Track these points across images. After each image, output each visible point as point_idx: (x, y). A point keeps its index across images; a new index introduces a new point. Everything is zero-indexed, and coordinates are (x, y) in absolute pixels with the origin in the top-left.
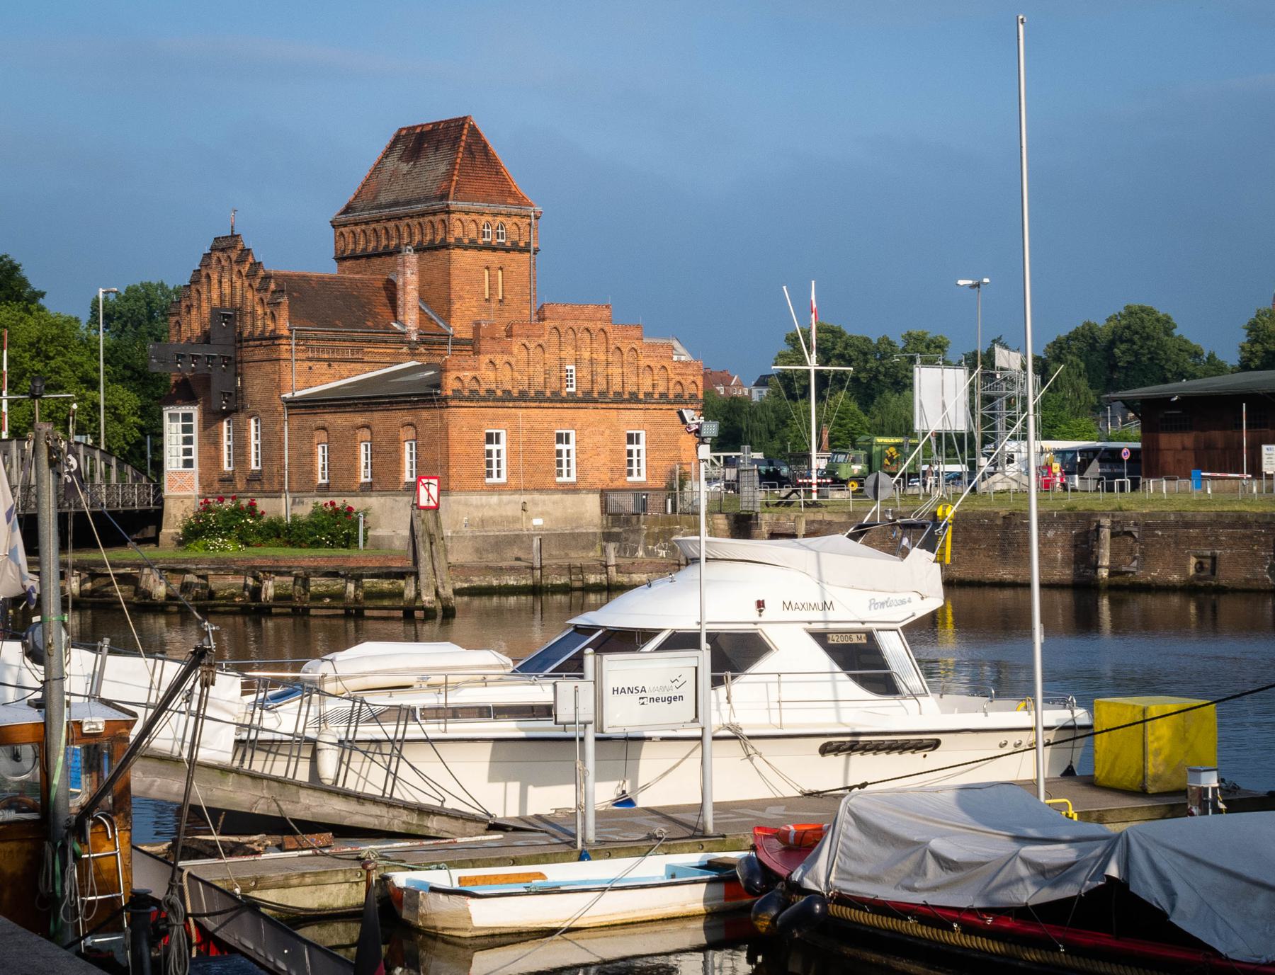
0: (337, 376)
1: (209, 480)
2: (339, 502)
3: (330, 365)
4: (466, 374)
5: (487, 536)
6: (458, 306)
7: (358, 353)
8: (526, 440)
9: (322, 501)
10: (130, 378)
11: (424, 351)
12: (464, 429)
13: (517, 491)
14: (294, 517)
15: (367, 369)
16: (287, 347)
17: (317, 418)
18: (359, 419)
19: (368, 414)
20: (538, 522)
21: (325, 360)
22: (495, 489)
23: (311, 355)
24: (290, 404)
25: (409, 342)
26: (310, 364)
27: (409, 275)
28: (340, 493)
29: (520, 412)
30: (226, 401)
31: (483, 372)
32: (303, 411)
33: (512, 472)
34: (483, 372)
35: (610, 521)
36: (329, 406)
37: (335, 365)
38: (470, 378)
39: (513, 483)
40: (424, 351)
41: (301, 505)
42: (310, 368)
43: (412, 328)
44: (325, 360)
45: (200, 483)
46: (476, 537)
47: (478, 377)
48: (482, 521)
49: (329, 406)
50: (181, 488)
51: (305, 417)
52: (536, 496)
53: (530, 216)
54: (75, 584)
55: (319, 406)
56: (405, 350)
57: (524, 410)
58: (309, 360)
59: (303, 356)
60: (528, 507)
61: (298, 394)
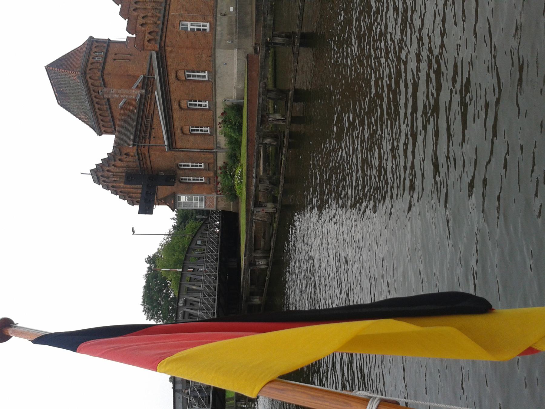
0: (159, 125)
1: (209, 189)
2: (219, 120)
3: (154, 129)
4: (146, 37)
5: (238, 32)
6: (131, 73)
7: (149, 116)
8: (186, 12)
9: (219, 130)
10: (184, 223)
11: (151, 88)
12: (178, 40)
13: (215, 18)
14: (223, 109)
15: (157, 112)
16: (142, 147)
17: (177, 132)
18: (175, 107)
19: (173, 102)
20: (232, 9)
21: (151, 131)
22: (213, 27)
23: (148, 137)
24: (171, 147)
25: (146, 93)
26: (152, 137)
27: (113, 92)
28: (214, 121)
29: (171, 13)
30: (170, 179)
31: (146, 29)
32: (173, 140)
33: (204, 20)
34: (146, 29)
35: (242, 401)
36: (170, 125)
37: (154, 126)
38: (149, 35)
39: (210, 19)
40: (151, 88)
41: (220, 143)
42: (154, 137)
43: (139, 92)
44: (151, 131)
45: (210, 194)
46: (239, 37)
47: (149, 32)
48: (230, 34)
49: (170, 125)
50: (212, 202)
51: (177, 139)
52: (218, 9)
53: (92, 41)
54: (260, 262)
55: (170, 131)
56: (149, 96)
57: (170, 12)
58: (150, 138)
59: (148, 140)
60: (223, 13)
61: (166, 143)
